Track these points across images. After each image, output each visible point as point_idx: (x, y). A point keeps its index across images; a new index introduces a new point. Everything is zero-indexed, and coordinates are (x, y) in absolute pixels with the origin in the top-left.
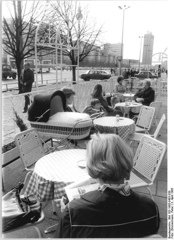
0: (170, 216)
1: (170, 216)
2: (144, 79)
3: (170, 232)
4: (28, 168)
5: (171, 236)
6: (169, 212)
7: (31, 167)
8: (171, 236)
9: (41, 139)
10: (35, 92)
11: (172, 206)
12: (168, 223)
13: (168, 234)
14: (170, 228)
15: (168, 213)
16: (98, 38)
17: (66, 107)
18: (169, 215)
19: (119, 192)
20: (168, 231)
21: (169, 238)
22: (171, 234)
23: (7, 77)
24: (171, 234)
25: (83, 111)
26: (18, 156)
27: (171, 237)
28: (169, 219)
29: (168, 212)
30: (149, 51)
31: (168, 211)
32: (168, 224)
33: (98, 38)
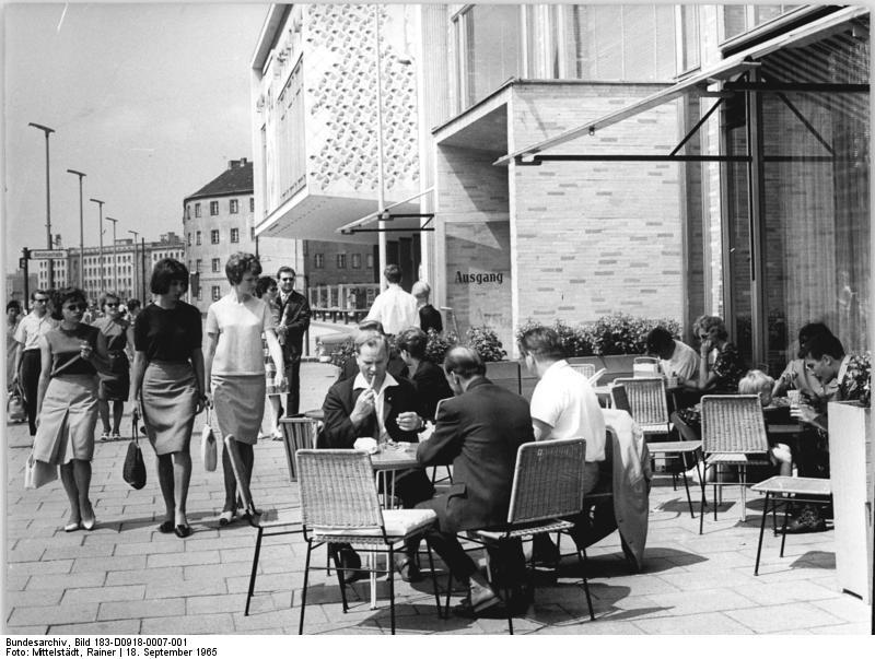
3: (31, 643)
5: (15, 648)
6: (102, 641)
8: (15, 648)
9: (787, 81)
11: (117, 653)
12: (63, 638)
14: (43, 643)
15: (99, 637)
16: (764, 565)
17: (810, 354)
19: (507, 621)
21: (8, 642)
22: (21, 648)
23: (116, 360)
24: (21, 648)
25: (748, 452)
31: (104, 637)
32: (57, 637)
33: (764, 565)
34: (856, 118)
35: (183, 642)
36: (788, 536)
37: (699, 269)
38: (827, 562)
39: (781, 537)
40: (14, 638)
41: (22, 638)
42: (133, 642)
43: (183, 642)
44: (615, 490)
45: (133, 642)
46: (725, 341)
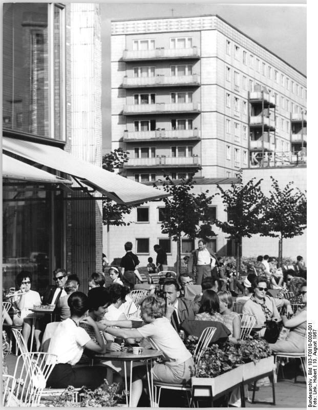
0: (310, 369)
1: (310, 369)
2: (60, 4)
3: (310, 396)
4: (214, 209)
5: (313, 403)
7: (170, 382)
8: (313, 403)
10: (167, 294)
13: (308, 399)
14: (311, 390)
15: (308, 364)
18: (310, 367)
20: (308, 395)
21: (310, 406)
22: (313, 400)
24: (313, 400)
26: (247, 93)
27: (312, 405)
28: (310, 374)
29: (307, 362)
30: (93, 145)
31: (308, 361)
34: (289, 197)
35: (310, 325)
36: (110, 226)
37: (7, 261)
38: (42, 349)
39: (107, 226)
40: (308, 403)
41: (308, 399)
42: (310, 348)
43: (310, 325)
44: (72, 102)
45: (310, 348)
46: (105, 275)
